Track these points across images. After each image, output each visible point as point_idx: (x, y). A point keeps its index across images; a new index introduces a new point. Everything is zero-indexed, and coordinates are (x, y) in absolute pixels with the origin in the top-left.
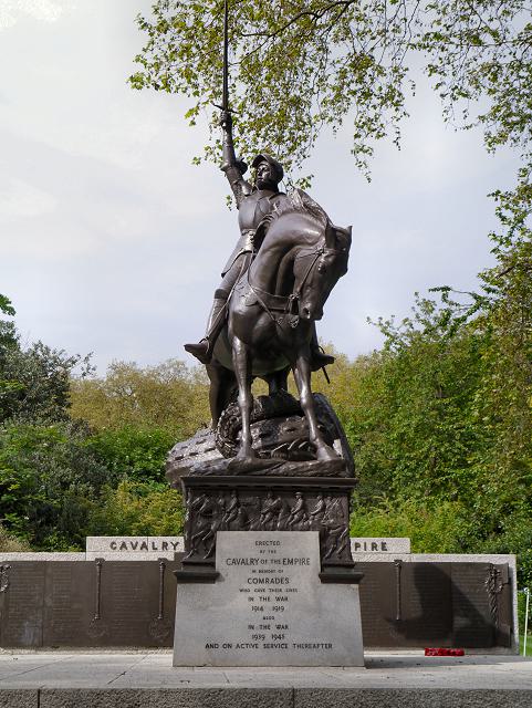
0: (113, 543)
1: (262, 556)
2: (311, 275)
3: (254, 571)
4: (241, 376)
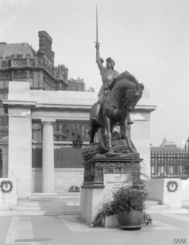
0: (93, 91)
1: (117, 181)
2: (88, 183)
3: (114, 185)
4: (109, 125)
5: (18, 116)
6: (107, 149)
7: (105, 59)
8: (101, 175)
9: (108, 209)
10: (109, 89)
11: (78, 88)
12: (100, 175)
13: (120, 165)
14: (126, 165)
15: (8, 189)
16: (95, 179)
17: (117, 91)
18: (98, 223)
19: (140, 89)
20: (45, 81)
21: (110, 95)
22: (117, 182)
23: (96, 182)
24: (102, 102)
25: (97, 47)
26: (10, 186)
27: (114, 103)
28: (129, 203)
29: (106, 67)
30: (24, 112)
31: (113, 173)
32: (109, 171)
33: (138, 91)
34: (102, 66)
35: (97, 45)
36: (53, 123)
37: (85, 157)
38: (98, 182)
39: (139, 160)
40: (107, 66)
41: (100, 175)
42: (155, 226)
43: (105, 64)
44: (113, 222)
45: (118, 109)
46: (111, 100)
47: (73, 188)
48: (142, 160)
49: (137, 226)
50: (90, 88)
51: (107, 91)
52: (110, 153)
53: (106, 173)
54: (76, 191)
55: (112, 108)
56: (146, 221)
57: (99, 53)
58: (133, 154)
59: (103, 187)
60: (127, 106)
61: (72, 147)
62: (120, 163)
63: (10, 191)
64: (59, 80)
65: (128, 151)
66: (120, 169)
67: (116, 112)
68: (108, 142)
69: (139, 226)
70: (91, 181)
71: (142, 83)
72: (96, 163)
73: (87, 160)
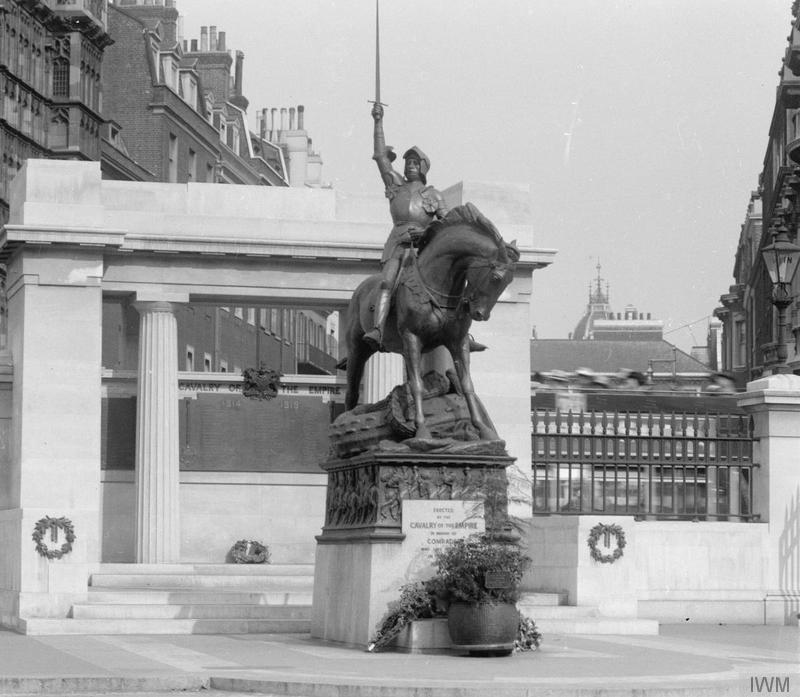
1: (440, 521)
3: (433, 533)
5: (60, 281)
6: (411, 426)
7: (400, 152)
8: (396, 502)
9: (420, 600)
10: (415, 246)
11: (152, 40)
12: (391, 504)
13: (448, 475)
14: (466, 474)
15: (58, 546)
16: (378, 515)
17: (441, 259)
18: (390, 640)
19: (510, 260)
20: (8, 26)
21: (419, 269)
22: (442, 525)
23: (379, 523)
24: (396, 287)
25: (378, 114)
26: (65, 535)
27: (433, 294)
28: (480, 580)
29: (403, 175)
30: (78, 268)
31: (429, 498)
32: (417, 492)
33: (503, 266)
34: (391, 173)
35: (378, 111)
36: (178, 309)
37: (341, 447)
38: (386, 523)
39: (501, 460)
40: (407, 171)
41: (391, 504)
42: (546, 652)
43: (399, 166)
44: (433, 638)
45: (444, 310)
46: (424, 281)
47: (245, 548)
48: (513, 460)
49: (501, 645)
50: (204, 30)
51: (408, 250)
52: (420, 440)
53: (410, 498)
54: (255, 557)
55: (427, 307)
56: (524, 640)
57: (382, 133)
58: (488, 442)
59: (400, 539)
60: (471, 303)
61: (239, 392)
62: (449, 470)
63: (66, 552)
64: (69, 17)
65: (471, 432)
66: (451, 486)
67: (439, 319)
68: (414, 403)
69: (506, 646)
70: (355, 516)
71: (514, 242)
72: (381, 468)
73: (348, 456)
